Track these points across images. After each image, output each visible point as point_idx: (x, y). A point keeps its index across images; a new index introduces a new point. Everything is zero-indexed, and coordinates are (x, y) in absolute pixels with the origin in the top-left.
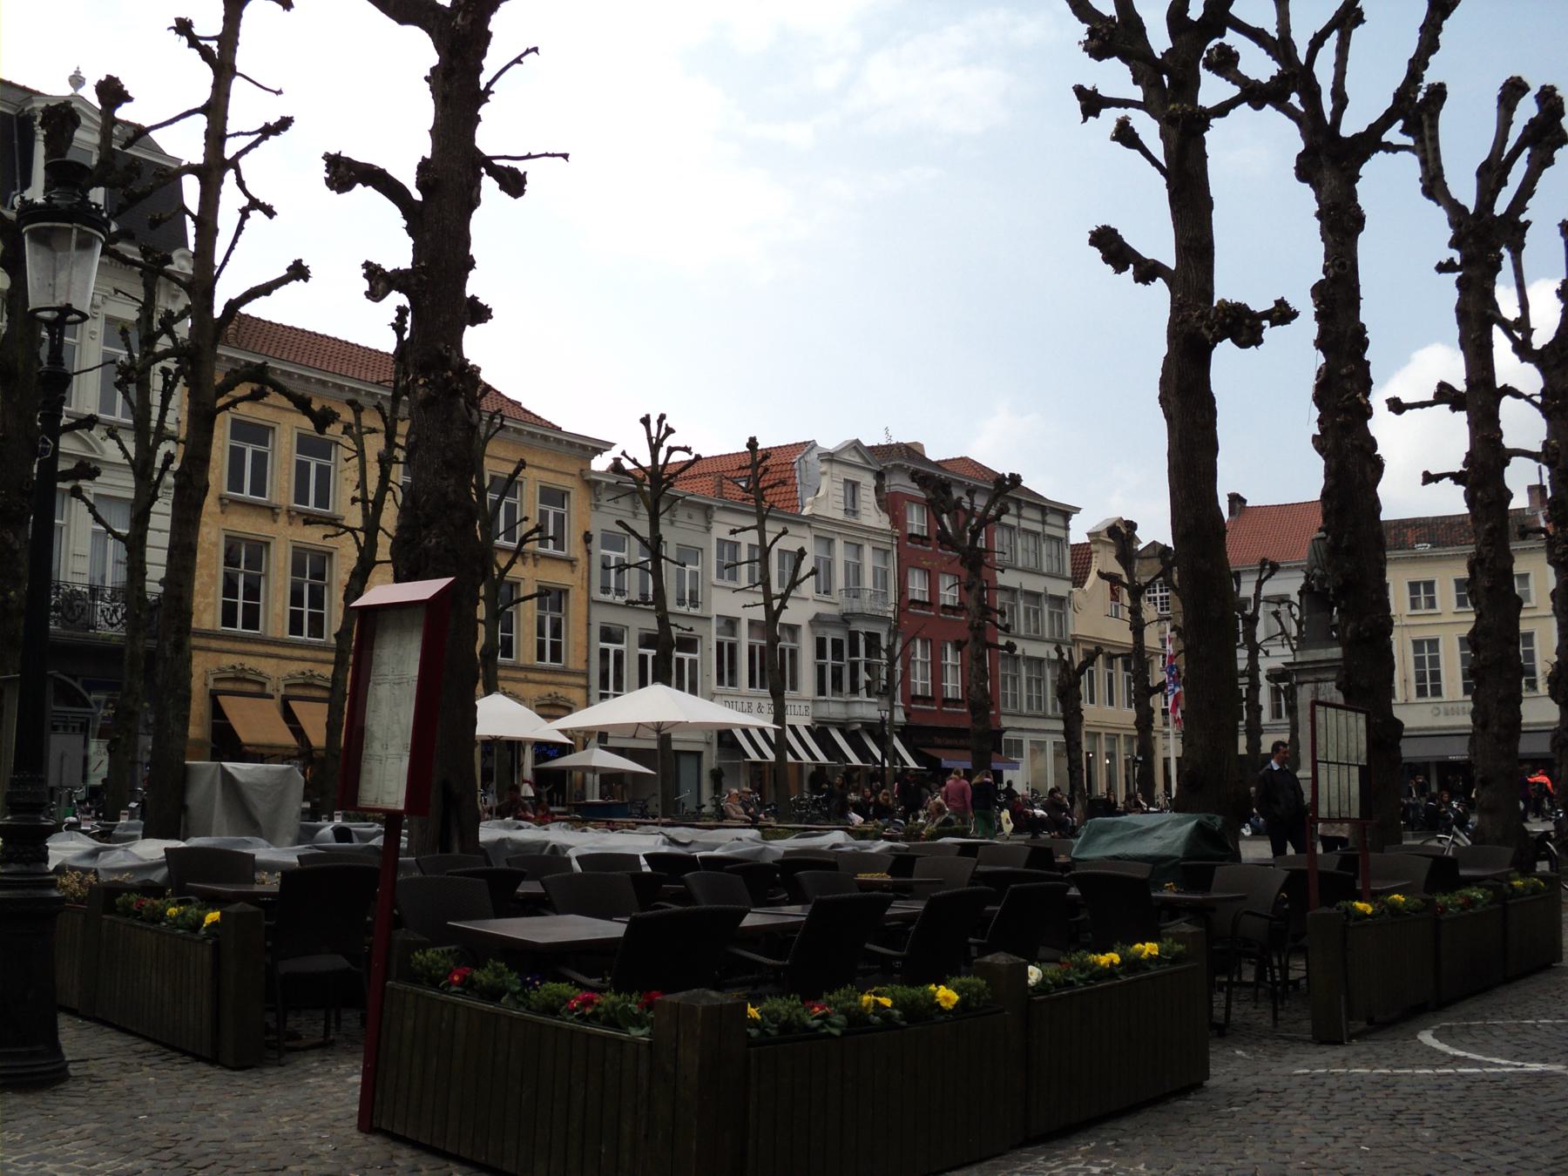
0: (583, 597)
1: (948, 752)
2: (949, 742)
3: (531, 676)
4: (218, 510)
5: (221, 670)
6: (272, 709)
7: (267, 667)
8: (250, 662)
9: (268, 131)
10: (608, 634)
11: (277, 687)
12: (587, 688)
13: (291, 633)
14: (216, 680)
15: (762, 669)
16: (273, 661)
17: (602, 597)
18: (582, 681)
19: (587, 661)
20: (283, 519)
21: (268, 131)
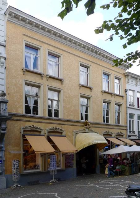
0: (125, 106)
1: (128, 101)
2: (55, 88)
3: (115, 127)
4: (22, 73)
5: (27, 128)
6: (44, 139)
7: (111, 131)
8: (36, 125)
9: (107, 40)
10: (132, 116)
11: (45, 132)
12: (127, 130)
13: (81, 120)
14: (24, 131)
15: (60, 70)
16: (44, 124)
17: (130, 107)
18: (125, 128)
19: (127, 123)
20: (45, 79)
21: (107, 40)
